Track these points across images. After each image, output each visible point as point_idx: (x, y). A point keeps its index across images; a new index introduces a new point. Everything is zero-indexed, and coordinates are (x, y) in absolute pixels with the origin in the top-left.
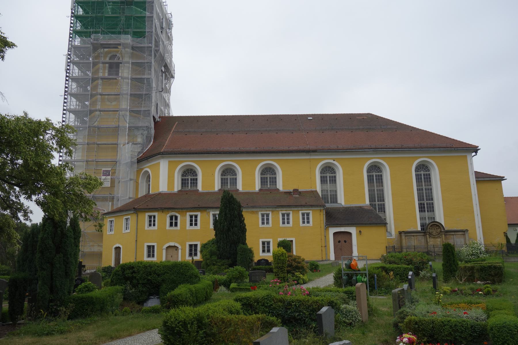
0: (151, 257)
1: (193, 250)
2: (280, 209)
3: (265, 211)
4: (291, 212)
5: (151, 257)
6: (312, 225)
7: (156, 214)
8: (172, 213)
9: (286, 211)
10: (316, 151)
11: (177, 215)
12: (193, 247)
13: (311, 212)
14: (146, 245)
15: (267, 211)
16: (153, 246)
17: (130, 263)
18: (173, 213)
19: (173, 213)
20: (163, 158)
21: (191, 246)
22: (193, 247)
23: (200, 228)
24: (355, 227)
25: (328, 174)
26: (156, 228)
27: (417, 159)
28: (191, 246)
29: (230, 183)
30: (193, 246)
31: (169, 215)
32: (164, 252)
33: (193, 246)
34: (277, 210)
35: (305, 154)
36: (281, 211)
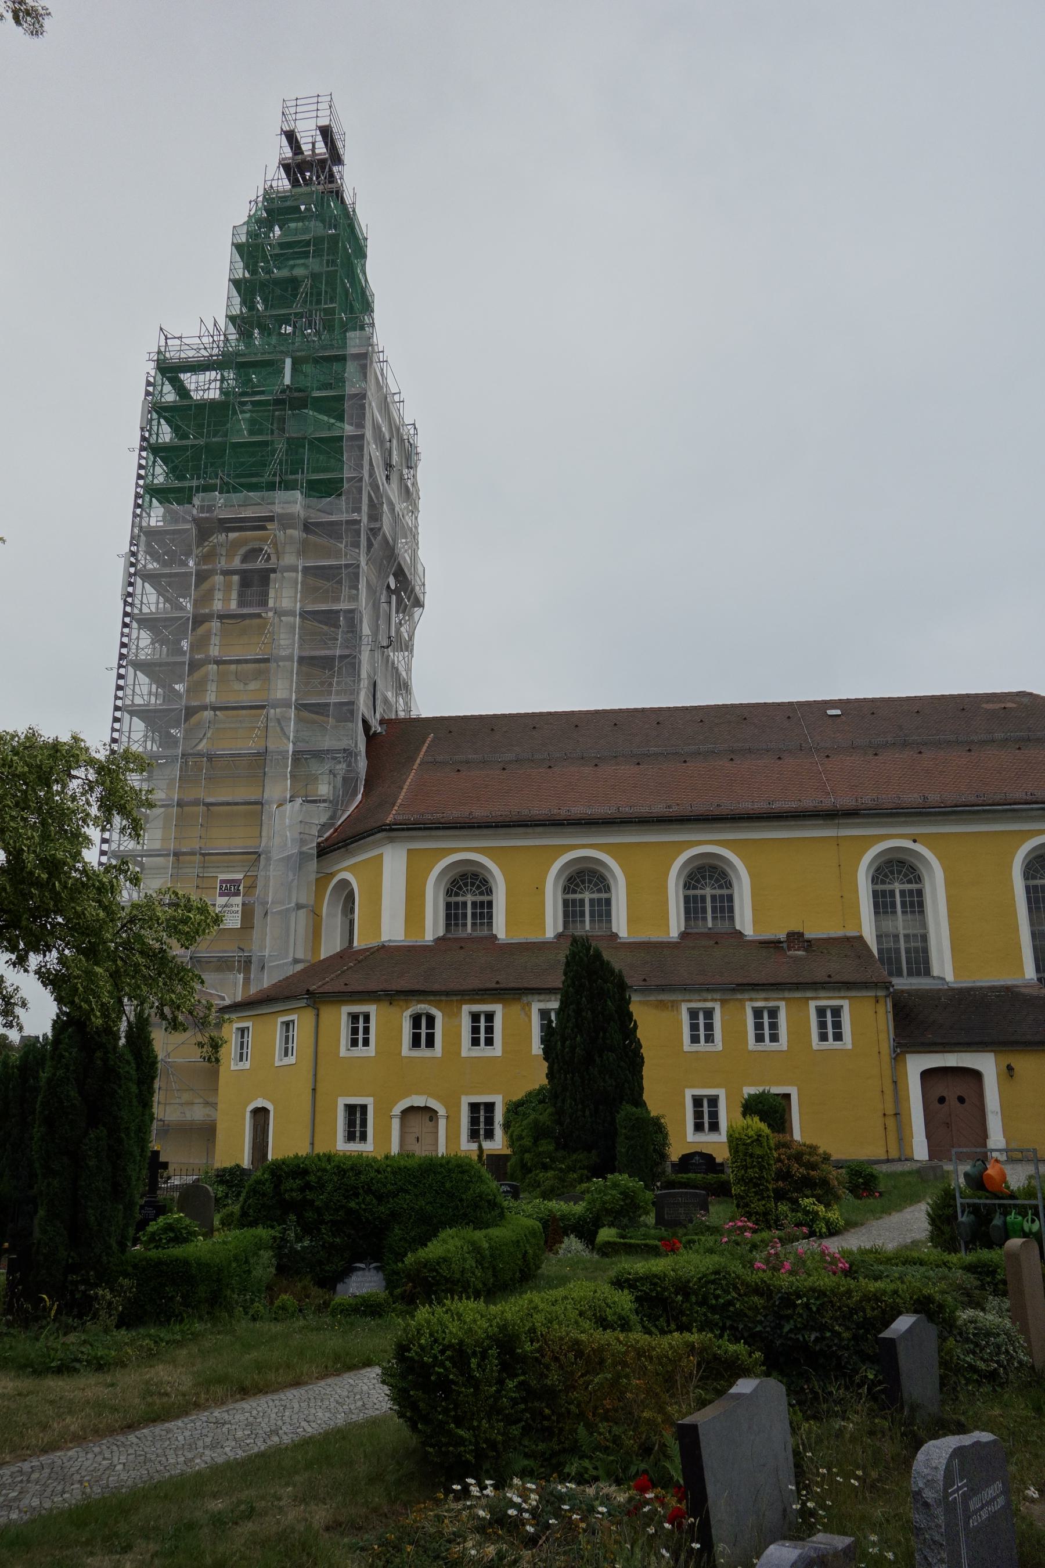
0: (358, 1139)
1: (482, 1119)
2: (747, 996)
3: (700, 1001)
4: (782, 1004)
5: (358, 1139)
6: (440, 1055)
7: (372, 1009)
8: (419, 1006)
9: (766, 999)
10: (857, 814)
11: (434, 1011)
12: (482, 1113)
13: (845, 1004)
14: (342, 1102)
15: (705, 1000)
16: (364, 1108)
17: (296, 1157)
18: (423, 1006)
19: (422, 1007)
20: (392, 840)
21: (474, 1107)
22: (482, 1113)
23: (376, 1053)
24: (992, 1055)
25: (708, 889)
26: (371, 1051)
27: (867, 850)
28: (474, 1107)
29: (592, 915)
30: (482, 1107)
31: (408, 1013)
32: (396, 1124)
33: (482, 1107)
34: (739, 996)
35: (821, 822)
36: (751, 1000)
